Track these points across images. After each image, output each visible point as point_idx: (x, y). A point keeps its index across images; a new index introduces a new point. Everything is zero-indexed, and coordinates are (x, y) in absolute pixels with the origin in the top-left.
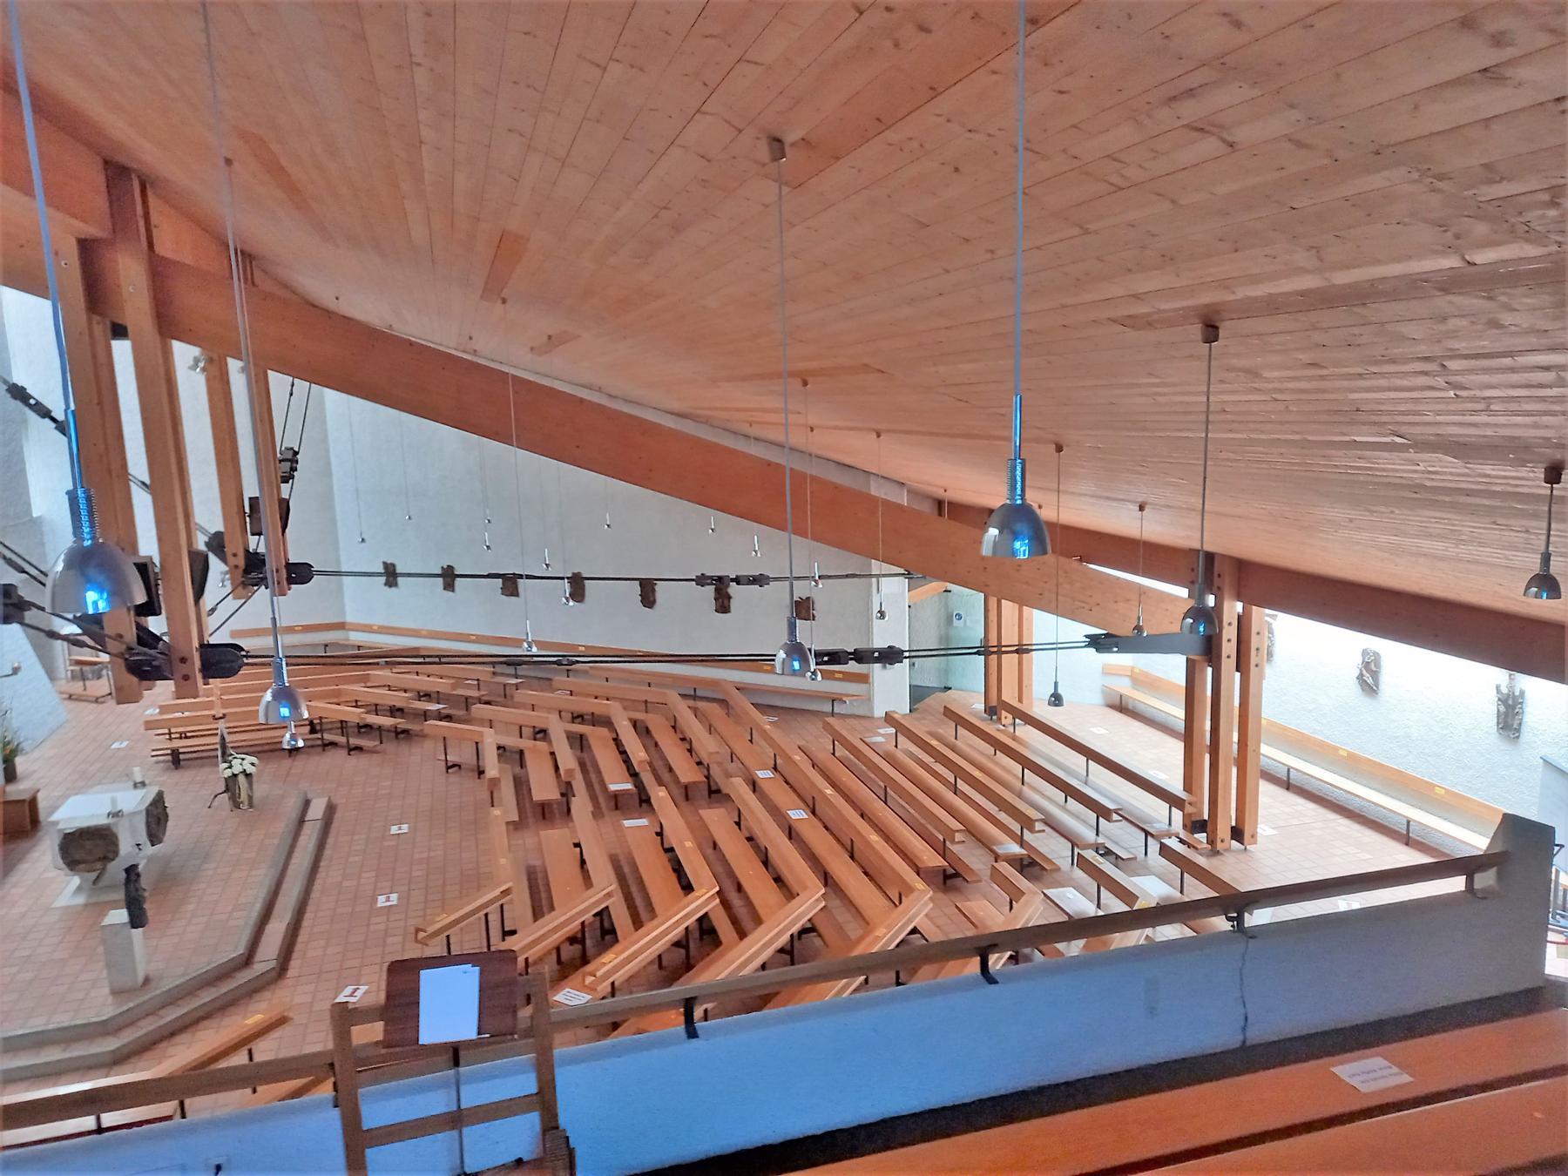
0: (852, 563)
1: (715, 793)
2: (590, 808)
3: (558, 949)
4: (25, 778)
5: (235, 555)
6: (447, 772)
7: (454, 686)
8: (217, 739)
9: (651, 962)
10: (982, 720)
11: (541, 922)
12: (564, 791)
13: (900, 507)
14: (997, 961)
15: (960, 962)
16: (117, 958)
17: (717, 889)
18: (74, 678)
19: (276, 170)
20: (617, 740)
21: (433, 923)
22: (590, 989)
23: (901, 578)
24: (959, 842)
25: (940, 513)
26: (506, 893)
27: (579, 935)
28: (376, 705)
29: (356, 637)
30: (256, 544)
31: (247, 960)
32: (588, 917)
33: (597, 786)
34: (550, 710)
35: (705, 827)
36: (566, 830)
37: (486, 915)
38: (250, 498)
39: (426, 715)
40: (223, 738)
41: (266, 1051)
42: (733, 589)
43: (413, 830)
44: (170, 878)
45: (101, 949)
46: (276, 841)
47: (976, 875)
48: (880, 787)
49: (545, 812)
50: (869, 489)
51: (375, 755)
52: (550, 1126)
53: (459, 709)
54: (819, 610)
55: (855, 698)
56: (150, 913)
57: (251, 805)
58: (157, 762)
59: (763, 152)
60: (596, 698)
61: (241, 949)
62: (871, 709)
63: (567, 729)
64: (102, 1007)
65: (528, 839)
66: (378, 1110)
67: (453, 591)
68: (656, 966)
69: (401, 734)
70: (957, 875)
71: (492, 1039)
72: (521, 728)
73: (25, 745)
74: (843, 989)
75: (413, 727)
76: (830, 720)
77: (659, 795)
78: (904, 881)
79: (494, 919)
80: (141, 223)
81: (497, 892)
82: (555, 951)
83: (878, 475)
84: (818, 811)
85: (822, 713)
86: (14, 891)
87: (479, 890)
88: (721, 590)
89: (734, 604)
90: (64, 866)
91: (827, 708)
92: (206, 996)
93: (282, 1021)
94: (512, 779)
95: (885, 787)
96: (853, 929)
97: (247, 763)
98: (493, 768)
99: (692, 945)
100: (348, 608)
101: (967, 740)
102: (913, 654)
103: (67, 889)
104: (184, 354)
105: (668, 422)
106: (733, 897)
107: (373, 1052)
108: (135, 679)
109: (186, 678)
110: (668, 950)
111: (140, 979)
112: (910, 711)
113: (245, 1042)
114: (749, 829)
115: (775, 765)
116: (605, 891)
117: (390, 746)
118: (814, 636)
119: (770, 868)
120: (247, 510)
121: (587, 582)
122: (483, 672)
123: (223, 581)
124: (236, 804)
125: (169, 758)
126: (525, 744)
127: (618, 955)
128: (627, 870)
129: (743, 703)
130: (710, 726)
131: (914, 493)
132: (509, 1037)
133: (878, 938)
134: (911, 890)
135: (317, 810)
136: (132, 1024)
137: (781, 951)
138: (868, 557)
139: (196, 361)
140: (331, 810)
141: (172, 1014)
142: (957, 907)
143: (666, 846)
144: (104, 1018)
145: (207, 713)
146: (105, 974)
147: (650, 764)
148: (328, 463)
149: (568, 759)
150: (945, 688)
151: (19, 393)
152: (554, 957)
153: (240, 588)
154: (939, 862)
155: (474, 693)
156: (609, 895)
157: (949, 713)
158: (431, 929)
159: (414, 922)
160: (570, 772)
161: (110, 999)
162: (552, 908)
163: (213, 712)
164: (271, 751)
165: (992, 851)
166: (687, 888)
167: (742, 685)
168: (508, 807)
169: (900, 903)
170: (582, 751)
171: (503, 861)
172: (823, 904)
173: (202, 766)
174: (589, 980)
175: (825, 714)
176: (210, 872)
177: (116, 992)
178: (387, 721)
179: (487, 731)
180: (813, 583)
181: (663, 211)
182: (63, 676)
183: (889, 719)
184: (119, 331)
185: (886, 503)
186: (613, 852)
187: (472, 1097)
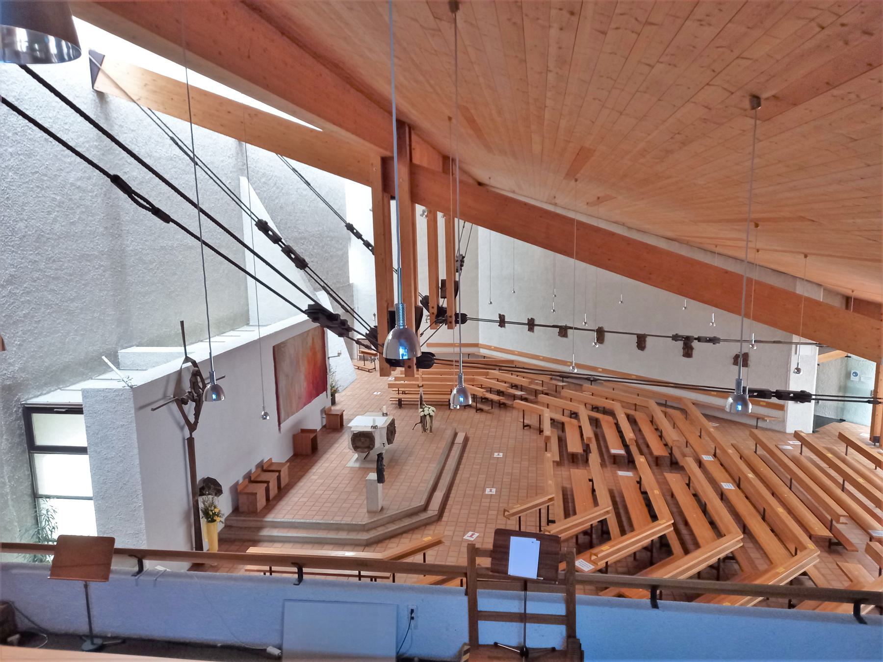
0: (779, 334)
1: (675, 465)
2: (599, 461)
3: (577, 537)
4: (338, 404)
5: (433, 308)
6: (524, 429)
7: (530, 383)
8: (419, 396)
9: (629, 556)
10: (867, 445)
11: (568, 520)
12: (585, 449)
13: (817, 303)
14: (866, 610)
15: (835, 604)
16: (371, 496)
17: (673, 521)
18: (360, 359)
19: (471, 122)
20: (617, 425)
21: (513, 508)
22: (594, 563)
23: (814, 346)
24: (843, 523)
25: (847, 307)
26: (551, 500)
27: (589, 531)
28: (491, 388)
29: (483, 351)
30: (443, 303)
31: (425, 508)
32: (595, 522)
33: (604, 450)
34: (580, 402)
35: (666, 483)
36: (586, 471)
37: (540, 510)
38: (442, 280)
39: (514, 397)
40: (421, 397)
41: (432, 557)
42: (695, 344)
43: (505, 456)
44: (395, 461)
45: (365, 490)
46: (441, 451)
47: (855, 547)
48: (787, 477)
49: (574, 460)
50: (795, 289)
51: (488, 414)
52: (571, 634)
53: (530, 396)
54: (752, 360)
55: (773, 419)
56: (386, 477)
57: (431, 431)
58: (392, 404)
59: (746, 104)
60: (606, 399)
61: (423, 503)
62: (784, 426)
63: (590, 414)
64: (363, 518)
65: (564, 472)
66: (487, 602)
67: (533, 332)
68: (632, 559)
69: (502, 406)
70: (839, 544)
71: (544, 581)
72: (563, 410)
73: (340, 389)
74: (751, 602)
75: (509, 402)
76: (756, 431)
77: (640, 460)
78: (800, 543)
79: (544, 512)
80: (408, 148)
81: (546, 498)
82: (575, 537)
83: (803, 279)
84: (742, 486)
85: (752, 427)
86: (332, 456)
87: (536, 495)
88: (687, 345)
89: (695, 353)
90: (352, 448)
91: (753, 422)
92: (407, 522)
93: (439, 543)
94: (557, 438)
95: (791, 479)
96: (762, 565)
97: (429, 410)
98: (548, 430)
99: (654, 550)
100: (481, 336)
101: (854, 456)
102: (819, 397)
103: (353, 459)
104: (419, 209)
105: (663, 245)
106: (682, 527)
107: (484, 572)
108: (388, 366)
109: (409, 367)
110: (640, 551)
111: (380, 508)
112: (813, 432)
113: (423, 549)
114: (695, 489)
115: (715, 453)
116: (605, 509)
117: (496, 411)
118: (753, 380)
119: (707, 515)
120: (440, 286)
121: (606, 334)
122: (546, 378)
123: (426, 320)
124: (425, 430)
125: (397, 402)
126: (565, 419)
127: (611, 547)
128: (618, 499)
129: (696, 413)
130: (674, 424)
131: (828, 291)
132: (554, 582)
133: (778, 574)
134: (804, 548)
135: (460, 439)
136: (375, 528)
137: (711, 567)
138: (790, 332)
139: (424, 212)
140: (466, 440)
141: (392, 527)
142: (838, 565)
143: (642, 490)
144: (364, 523)
145: (414, 382)
146: (365, 502)
147: (636, 441)
148: (477, 263)
149: (588, 431)
150: (841, 420)
151: (350, 227)
152: (574, 540)
153: (434, 324)
154: (826, 533)
155: (540, 388)
156: (607, 512)
157: (842, 437)
158: (512, 511)
159: (503, 506)
160: (589, 439)
161: (367, 515)
162: (575, 513)
163: (417, 383)
164: (442, 405)
165: (869, 534)
166: (654, 517)
167: (695, 402)
168: (553, 454)
169: (796, 554)
170: (596, 428)
171: (550, 482)
172: (742, 544)
173: (411, 408)
174: (594, 558)
175: (751, 426)
176: (412, 461)
177: (369, 512)
178: (495, 397)
179: (545, 409)
180: (751, 346)
181: (677, 135)
182: (356, 358)
183: (797, 435)
184: (393, 198)
185: (808, 300)
186: (610, 488)
187: (533, 608)
